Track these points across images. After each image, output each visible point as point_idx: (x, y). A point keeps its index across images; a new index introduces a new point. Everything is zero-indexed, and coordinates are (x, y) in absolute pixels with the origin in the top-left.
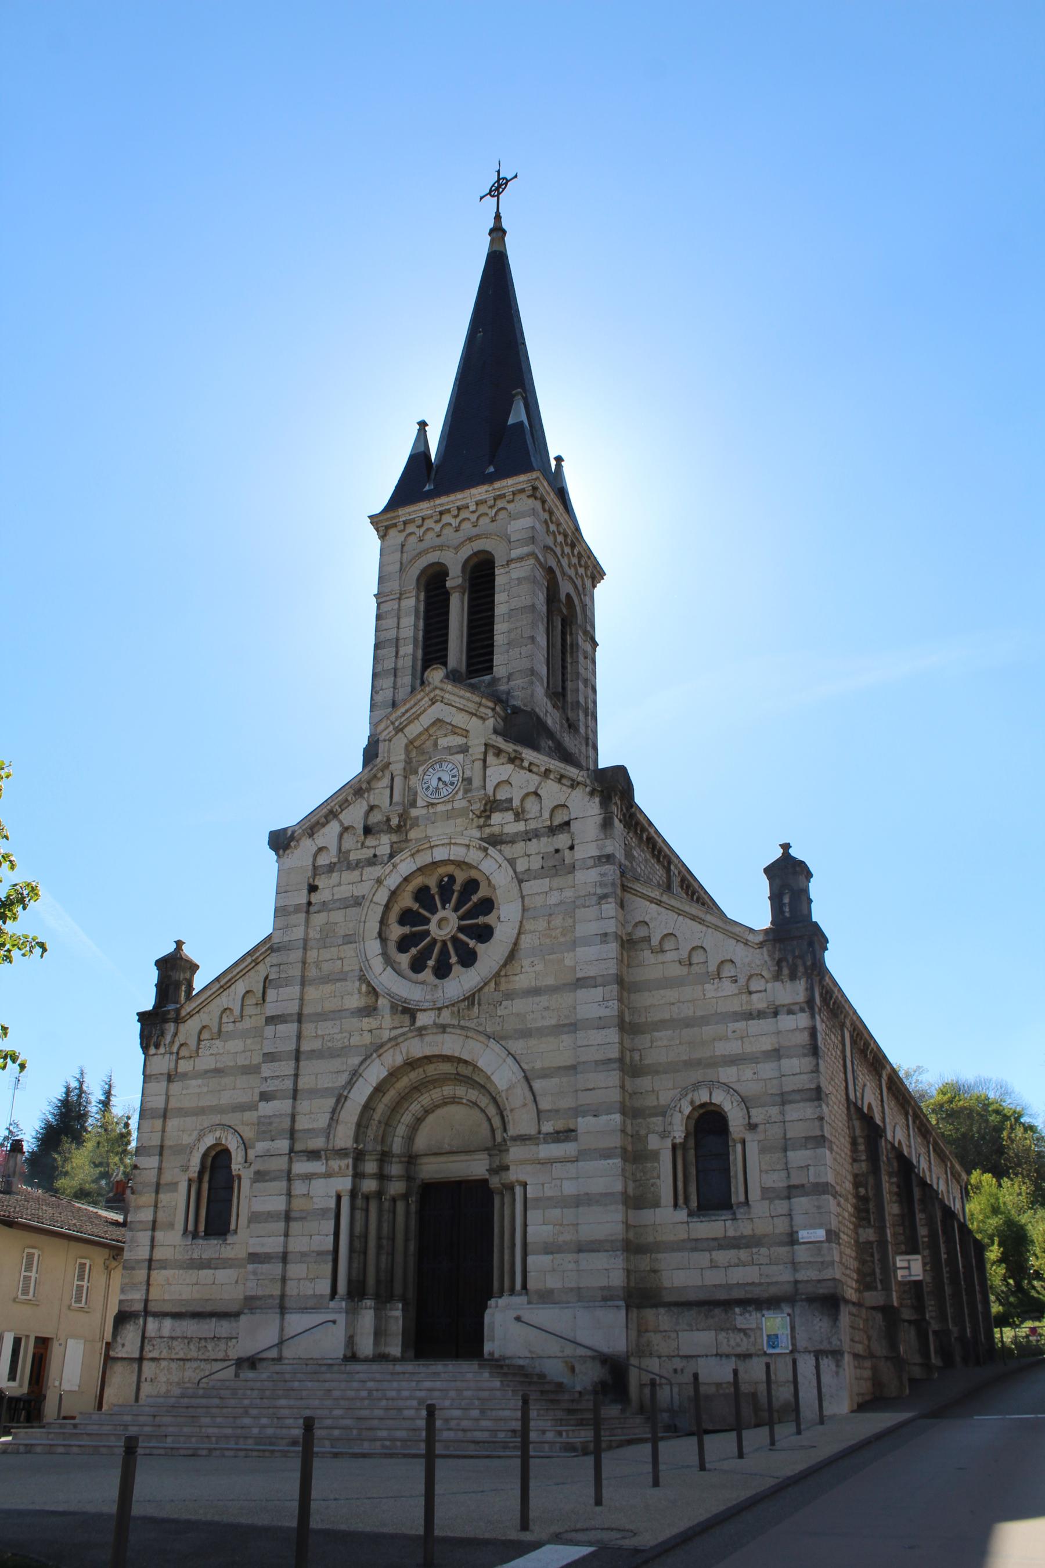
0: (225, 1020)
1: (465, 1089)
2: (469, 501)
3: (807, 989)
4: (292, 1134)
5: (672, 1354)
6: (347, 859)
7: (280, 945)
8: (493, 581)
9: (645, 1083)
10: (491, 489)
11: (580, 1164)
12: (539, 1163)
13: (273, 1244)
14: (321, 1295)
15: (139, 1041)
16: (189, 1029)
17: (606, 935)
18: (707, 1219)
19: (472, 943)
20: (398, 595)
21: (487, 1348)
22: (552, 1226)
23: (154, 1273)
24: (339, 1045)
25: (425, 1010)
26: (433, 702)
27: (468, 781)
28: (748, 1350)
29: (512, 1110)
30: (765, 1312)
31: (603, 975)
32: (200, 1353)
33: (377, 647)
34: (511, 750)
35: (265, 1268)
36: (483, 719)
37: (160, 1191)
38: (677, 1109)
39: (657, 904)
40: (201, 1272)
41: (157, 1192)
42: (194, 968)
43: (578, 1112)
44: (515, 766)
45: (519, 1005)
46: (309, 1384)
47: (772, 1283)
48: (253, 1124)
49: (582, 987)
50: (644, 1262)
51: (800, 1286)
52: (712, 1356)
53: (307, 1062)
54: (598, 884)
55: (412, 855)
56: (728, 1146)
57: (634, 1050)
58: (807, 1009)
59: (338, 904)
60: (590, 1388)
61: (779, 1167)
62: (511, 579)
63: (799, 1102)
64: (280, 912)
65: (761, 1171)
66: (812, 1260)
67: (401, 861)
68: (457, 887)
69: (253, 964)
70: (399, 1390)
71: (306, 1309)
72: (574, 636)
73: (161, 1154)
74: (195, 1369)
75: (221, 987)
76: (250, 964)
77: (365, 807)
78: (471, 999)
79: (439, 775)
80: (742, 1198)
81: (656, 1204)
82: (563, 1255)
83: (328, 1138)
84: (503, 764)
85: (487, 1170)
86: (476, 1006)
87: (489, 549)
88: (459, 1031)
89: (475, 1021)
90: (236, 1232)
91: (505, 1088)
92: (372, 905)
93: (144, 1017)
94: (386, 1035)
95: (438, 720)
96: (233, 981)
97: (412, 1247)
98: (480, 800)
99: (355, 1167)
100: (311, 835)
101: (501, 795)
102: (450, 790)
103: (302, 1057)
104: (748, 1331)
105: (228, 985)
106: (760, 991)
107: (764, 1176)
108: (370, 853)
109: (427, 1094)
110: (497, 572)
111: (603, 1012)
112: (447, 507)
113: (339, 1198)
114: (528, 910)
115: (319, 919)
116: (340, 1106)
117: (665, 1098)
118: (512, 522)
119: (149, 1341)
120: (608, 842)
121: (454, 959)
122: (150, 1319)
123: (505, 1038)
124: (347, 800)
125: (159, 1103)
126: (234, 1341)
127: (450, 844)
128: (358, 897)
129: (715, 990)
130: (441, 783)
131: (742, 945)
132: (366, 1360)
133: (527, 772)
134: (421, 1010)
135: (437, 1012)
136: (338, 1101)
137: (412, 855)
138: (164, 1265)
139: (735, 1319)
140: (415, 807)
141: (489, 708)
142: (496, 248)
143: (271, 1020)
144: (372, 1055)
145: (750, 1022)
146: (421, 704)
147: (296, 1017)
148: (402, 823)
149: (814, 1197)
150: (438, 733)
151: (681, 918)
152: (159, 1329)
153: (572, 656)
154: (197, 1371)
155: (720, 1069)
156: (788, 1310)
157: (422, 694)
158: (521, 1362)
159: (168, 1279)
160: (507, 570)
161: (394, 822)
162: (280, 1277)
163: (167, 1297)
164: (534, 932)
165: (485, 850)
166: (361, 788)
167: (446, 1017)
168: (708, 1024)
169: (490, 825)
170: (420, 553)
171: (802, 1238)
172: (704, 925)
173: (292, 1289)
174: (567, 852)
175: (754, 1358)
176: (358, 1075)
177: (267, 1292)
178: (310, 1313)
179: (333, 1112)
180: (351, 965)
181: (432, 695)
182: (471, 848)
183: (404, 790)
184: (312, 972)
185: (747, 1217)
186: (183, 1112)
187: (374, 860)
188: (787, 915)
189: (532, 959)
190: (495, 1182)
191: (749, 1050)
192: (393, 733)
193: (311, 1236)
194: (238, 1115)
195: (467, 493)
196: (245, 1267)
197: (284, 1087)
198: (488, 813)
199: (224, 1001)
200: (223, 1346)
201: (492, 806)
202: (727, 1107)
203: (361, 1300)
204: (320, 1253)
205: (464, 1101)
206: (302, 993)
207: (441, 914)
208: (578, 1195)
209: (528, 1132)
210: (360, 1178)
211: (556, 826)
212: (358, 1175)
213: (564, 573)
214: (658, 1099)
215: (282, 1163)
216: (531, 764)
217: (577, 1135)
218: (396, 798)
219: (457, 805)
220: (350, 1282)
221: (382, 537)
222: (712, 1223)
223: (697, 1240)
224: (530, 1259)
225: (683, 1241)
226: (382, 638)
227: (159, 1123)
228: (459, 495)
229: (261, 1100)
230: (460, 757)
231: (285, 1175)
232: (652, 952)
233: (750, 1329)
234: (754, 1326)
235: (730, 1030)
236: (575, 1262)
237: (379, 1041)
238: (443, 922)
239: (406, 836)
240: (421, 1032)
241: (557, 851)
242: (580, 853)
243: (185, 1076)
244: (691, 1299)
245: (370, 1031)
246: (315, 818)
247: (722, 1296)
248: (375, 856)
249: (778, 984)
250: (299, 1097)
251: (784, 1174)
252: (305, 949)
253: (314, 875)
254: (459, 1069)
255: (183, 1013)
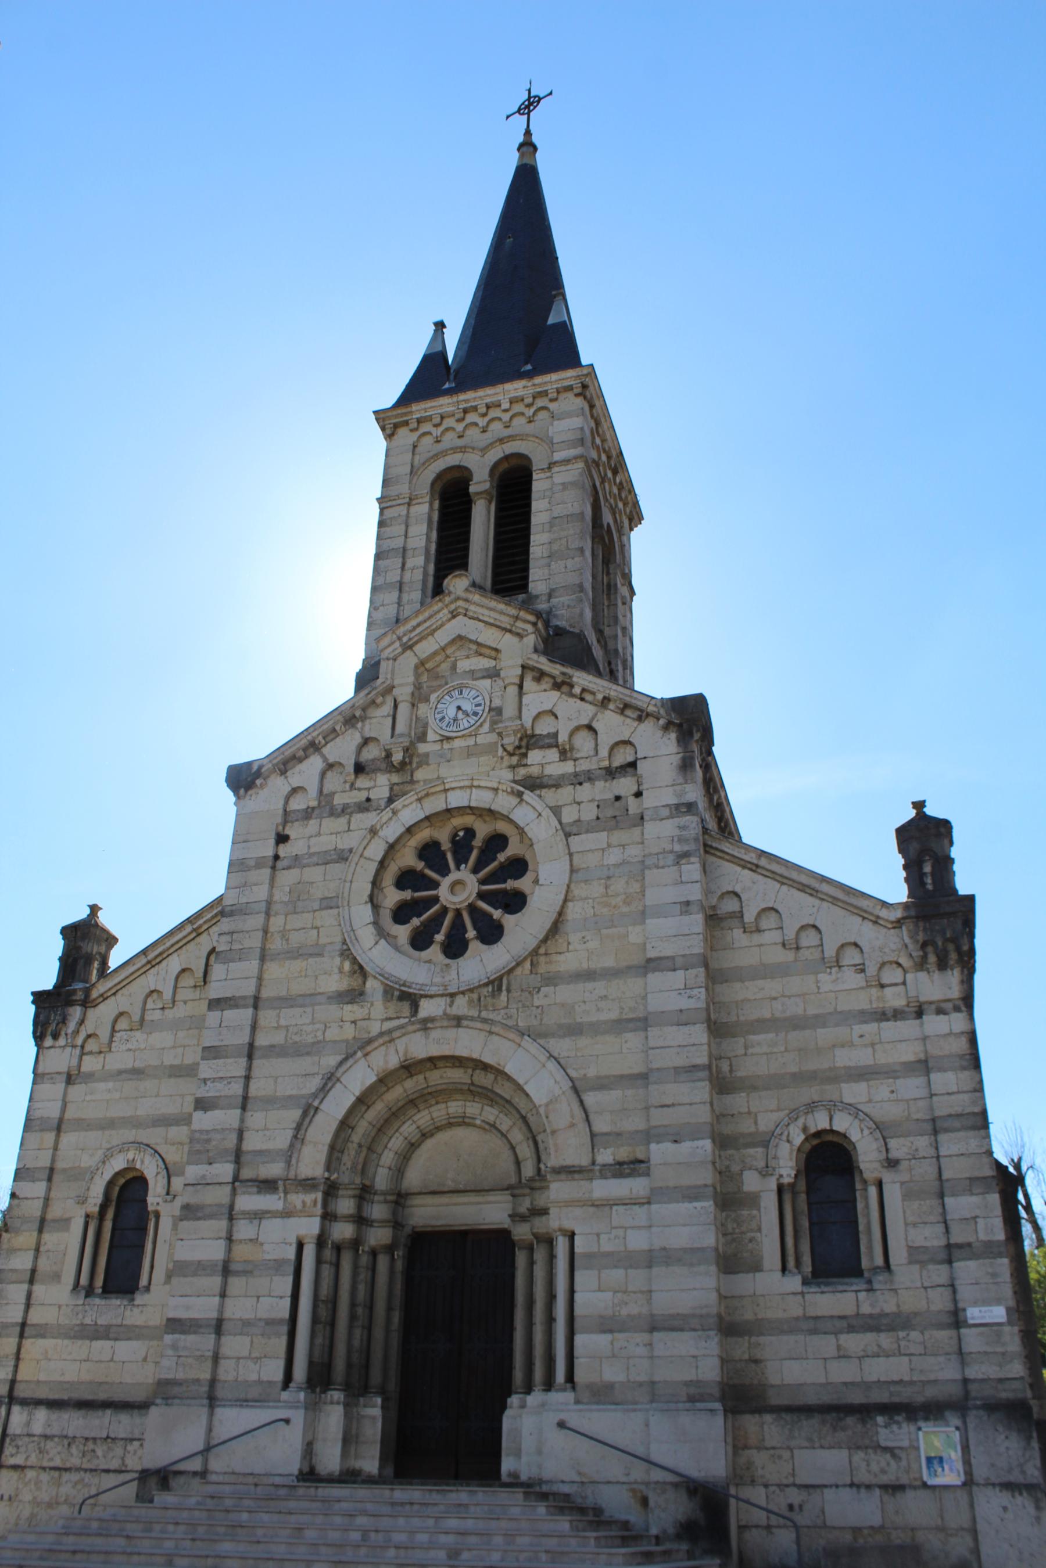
0: (150, 1005)
1: (480, 1105)
2: (501, 397)
3: (962, 982)
4: (238, 1156)
5: (785, 1482)
6: (330, 803)
7: (234, 908)
8: (529, 490)
9: (738, 1101)
10: (530, 384)
11: (654, 1207)
12: (593, 1205)
13: (205, 1308)
14: (270, 1382)
15: (31, 1028)
16: (100, 1017)
17: (688, 903)
18: (830, 1289)
19: (497, 914)
20: (407, 500)
21: (507, 1465)
22: (611, 1294)
23: (27, 1343)
24: (310, 1039)
25: (431, 997)
26: (454, 615)
27: (499, 711)
28: (898, 1479)
29: (553, 1132)
30: (921, 1424)
31: (684, 956)
32: (85, 1460)
33: (378, 557)
34: (558, 673)
35: (189, 1340)
36: (520, 636)
37: (45, 1230)
38: (784, 1137)
39: (751, 870)
40: (94, 1343)
41: (40, 1231)
42: (111, 941)
43: (649, 1136)
44: (562, 693)
45: (565, 993)
46: (265, 1517)
47: (929, 1382)
48: (181, 1144)
49: (654, 970)
50: (741, 1349)
51: (973, 1388)
52: (845, 1486)
53: (264, 1061)
54: (676, 839)
55: (419, 800)
56: (854, 1190)
57: (721, 1058)
58: (963, 1008)
59: (315, 859)
60: (671, 1531)
61: (932, 1219)
62: (553, 484)
63: (958, 1130)
64: (236, 866)
65: (906, 1224)
66: (989, 1349)
67: (405, 806)
68: (477, 842)
69: (194, 935)
70: (412, 1533)
71: (246, 1401)
72: (612, 576)
73: (50, 1179)
74: (76, 1483)
75: (149, 962)
76: (189, 934)
77: (357, 739)
78: (496, 984)
79: (459, 703)
80: (879, 1261)
81: (756, 1267)
82: (627, 1334)
83: (288, 1163)
84: (545, 690)
85: (510, 1216)
86: (504, 993)
87: (526, 452)
88: (479, 1025)
89: (503, 1012)
90: (147, 1289)
91: (544, 1101)
92: (362, 860)
93: (40, 998)
94: (375, 1028)
95: (460, 637)
96: (165, 955)
97: (396, 1318)
98: (515, 732)
99: (325, 1204)
100: (283, 772)
101: (544, 728)
102: (473, 722)
103: (257, 1054)
104: (897, 1451)
105: (158, 960)
106: (896, 985)
107: (912, 1231)
108: (362, 796)
109: (427, 1112)
110: (535, 476)
111: (685, 1003)
112: (473, 404)
113: (300, 1246)
114: (578, 871)
115: (287, 878)
116: (307, 1120)
117: (766, 1123)
118: (556, 423)
119: (12, 1440)
120: (689, 787)
121: (471, 933)
122: (16, 1409)
123: (545, 1035)
124: (334, 730)
125: (53, 1111)
126: (136, 1444)
127: (471, 787)
128: (343, 850)
129: (834, 981)
130: (460, 712)
131: (870, 924)
132: (331, 1480)
133: (579, 701)
134: (426, 996)
135: (448, 999)
136: (305, 1114)
137: (419, 800)
138: (43, 1332)
139: (877, 1433)
140: (425, 741)
141: (529, 622)
142: (526, 161)
143: (215, 1004)
144: (355, 1053)
145: (884, 1024)
146: (438, 616)
147: (251, 1001)
148: (407, 760)
149: (987, 1261)
150: (458, 654)
151: (785, 888)
152: (28, 1424)
153: (609, 599)
154: (79, 1487)
155: (843, 1085)
156: (955, 1421)
157: (440, 604)
158: (566, 1489)
159: (47, 1352)
160: (548, 474)
161: (397, 757)
162: (211, 1354)
163: (42, 1377)
164: (586, 899)
165: (520, 795)
166: (354, 716)
167: (461, 1006)
168: (824, 1026)
169: (526, 765)
170: (436, 455)
171: (973, 1318)
172: (816, 897)
173: (227, 1371)
174: (631, 800)
175: (907, 1491)
176: (334, 1079)
177: (192, 1375)
178: (252, 1406)
179: (298, 1128)
180: (331, 936)
181: (453, 607)
182: (500, 792)
183: (411, 720)
184: (276, 944)
185: (888, 1287)
186: (84, 1125)
187: (367, 805)
188: (930, 887)
189: (584, 934)
190: (521, 1232)
191: (883, 1061)
192: (400, 650)
193: (258, 1297)
194: (160, 1131)
195: (499, 388)
196: (161, 1338)
197: (231, 1093)
198: (523, 750)
199: (150, 980)
200: (119, 1451)
201: (529, 741)
202: (855, 1136)
203: (324, 1392)
204: (270, 1322)
205: (478, 1122)
206: (261, 971)
207: (454, 876)
208: (650, 1251)
209: (576, 1162)
210: (330, 1221)
211: (617, 768)
212: (328, 1216)
213: (606, 500)
214: (756, 1123)
215: (222, 1195)
216: (584, 690)
217: (649, 1168)
218: (400, 728)
219: (480, 740)
220: (311, 1364)
221: (389, 436)
222: (839, 1295)
223: (816, 1318)
224: (579, 1339)
225: (797, 1319)
226: (385, 547)
227: (50, 1137)
228: (489, 391)
229: (196, 1109)
230: (487, 682)
231: (226, 1211)
232: (745, 932)
233: (901, 1448)
234: (905, 1443)
235: (855, 1034)
236: (645, 1345)
237: (366, 1036)
238: (458, 888)
239: (412, 776)
240: (426, 1025)
241: (618, 798)
242: (649, 800)
243: (90, 1077)
244: (810, 1403)
245: (354, 1022)
246: (290, 751)
247: (857, 1398)
248: (368, 800)
249: (922, 976)
250: (249, 1106)
251: (941, 1228)
252: (268, 914)
253: (285, 822)
254: (476, 1079)
255: (94, 994)
